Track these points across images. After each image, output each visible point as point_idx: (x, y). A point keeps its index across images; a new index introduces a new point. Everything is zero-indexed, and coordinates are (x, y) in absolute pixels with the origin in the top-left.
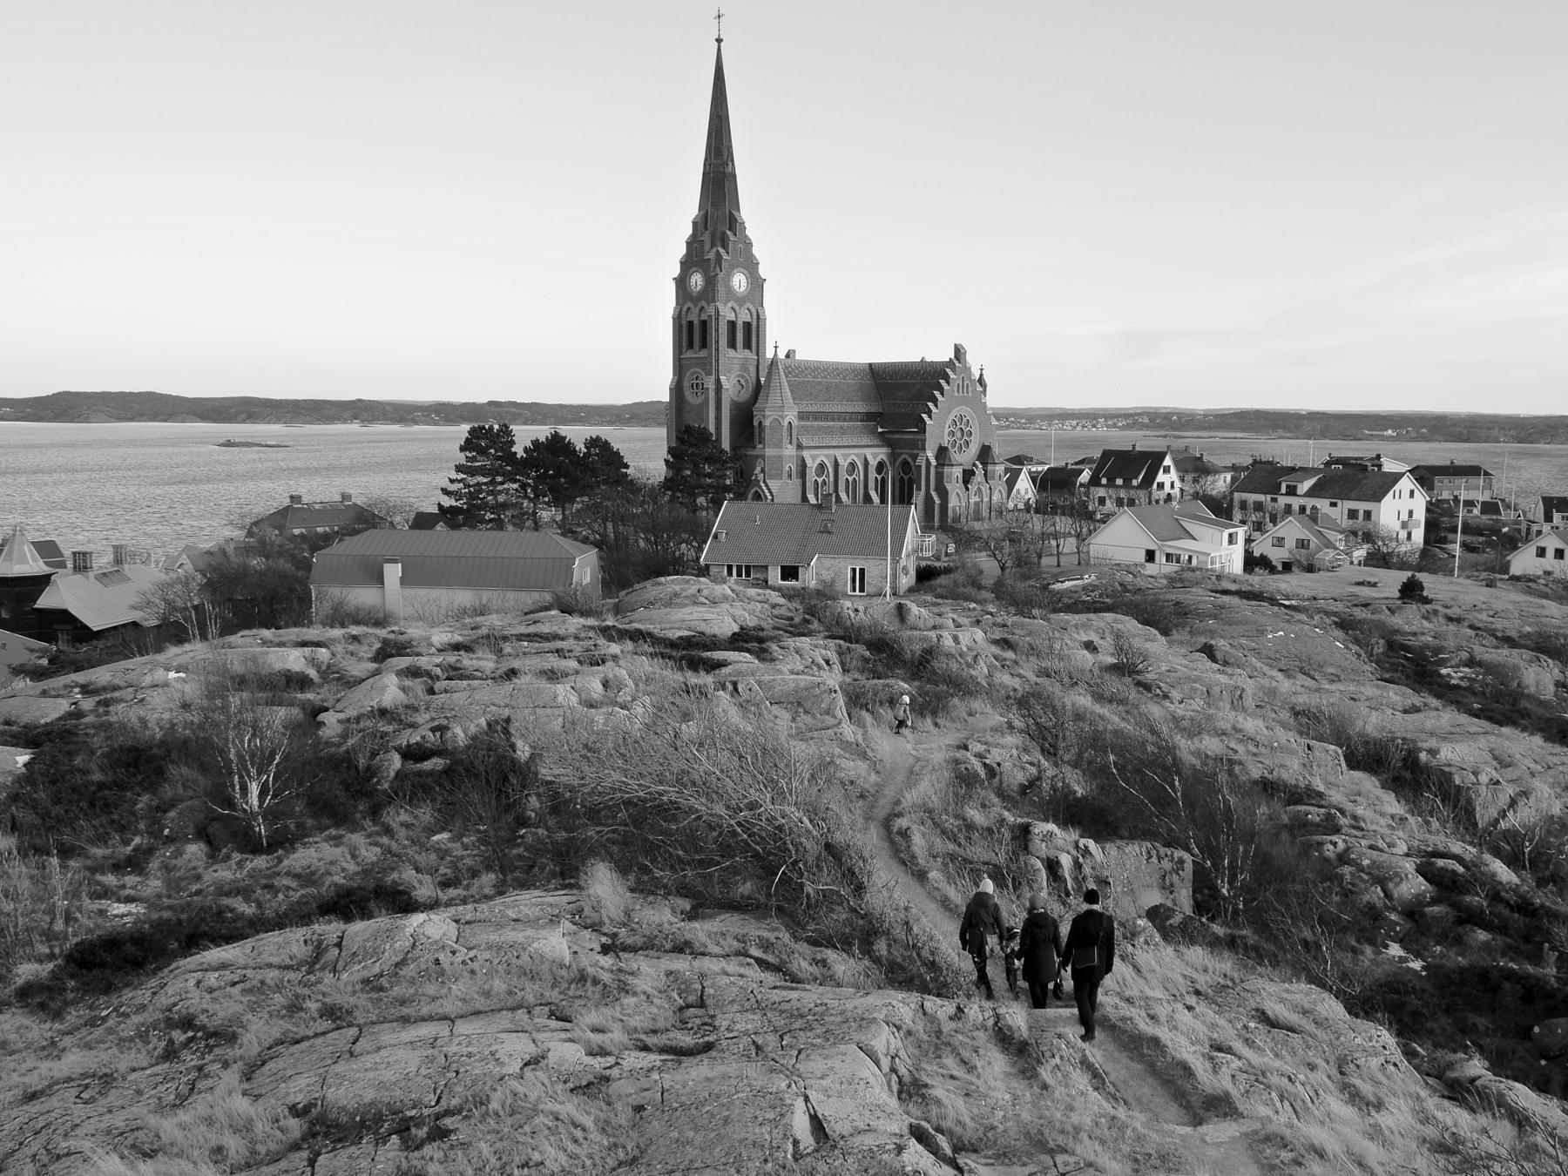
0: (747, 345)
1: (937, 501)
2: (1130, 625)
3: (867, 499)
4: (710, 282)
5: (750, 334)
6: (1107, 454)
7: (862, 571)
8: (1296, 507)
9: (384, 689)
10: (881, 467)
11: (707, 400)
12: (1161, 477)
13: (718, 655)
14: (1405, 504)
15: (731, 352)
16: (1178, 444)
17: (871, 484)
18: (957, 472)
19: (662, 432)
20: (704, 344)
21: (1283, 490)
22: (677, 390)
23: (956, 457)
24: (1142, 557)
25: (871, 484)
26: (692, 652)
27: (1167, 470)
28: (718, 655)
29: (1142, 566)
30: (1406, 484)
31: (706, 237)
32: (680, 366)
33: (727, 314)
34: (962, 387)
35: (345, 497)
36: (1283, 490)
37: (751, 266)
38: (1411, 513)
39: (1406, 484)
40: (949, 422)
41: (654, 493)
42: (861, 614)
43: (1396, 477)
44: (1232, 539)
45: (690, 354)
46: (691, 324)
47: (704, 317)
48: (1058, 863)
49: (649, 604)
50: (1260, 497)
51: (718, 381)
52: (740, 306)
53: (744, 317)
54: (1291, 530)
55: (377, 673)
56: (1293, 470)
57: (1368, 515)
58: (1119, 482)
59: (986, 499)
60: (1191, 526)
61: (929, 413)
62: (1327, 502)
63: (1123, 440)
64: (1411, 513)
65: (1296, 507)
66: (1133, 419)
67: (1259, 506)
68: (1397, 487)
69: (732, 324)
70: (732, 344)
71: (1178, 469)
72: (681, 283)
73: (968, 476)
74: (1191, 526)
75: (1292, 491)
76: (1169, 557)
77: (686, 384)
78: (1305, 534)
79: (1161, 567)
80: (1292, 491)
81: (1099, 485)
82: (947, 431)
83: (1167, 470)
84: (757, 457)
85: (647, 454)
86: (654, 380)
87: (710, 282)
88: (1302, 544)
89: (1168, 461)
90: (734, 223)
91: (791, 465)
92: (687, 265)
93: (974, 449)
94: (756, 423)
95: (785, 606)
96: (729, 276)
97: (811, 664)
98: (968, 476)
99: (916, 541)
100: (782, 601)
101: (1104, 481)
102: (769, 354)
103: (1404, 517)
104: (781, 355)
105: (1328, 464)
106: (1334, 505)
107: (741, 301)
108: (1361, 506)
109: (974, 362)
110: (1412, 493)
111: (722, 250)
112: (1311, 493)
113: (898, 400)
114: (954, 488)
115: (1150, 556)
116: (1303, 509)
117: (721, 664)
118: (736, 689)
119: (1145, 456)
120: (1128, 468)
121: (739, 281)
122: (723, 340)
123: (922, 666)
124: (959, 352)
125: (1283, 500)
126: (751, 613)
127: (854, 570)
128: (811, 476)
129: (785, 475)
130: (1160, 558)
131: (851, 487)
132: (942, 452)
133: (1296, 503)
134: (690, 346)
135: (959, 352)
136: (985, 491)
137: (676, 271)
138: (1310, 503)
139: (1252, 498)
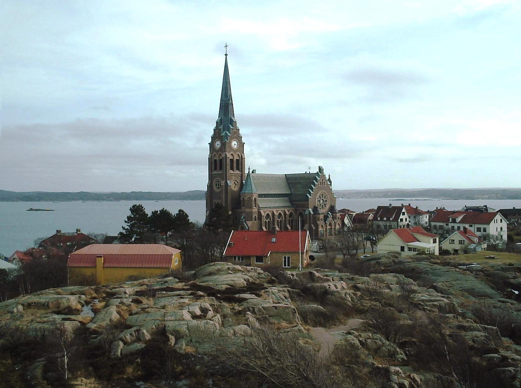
0: (238, 169)
1: (314, 228)
2: (402, 277)
3: (286, 229)
4: (223, 145)
5: (239, 164)
6: (379, 208)
7: (289, 258)
8: (456, 228)
9: (111, 313)
10: (291, 215)
11: (222, 190)
12: (401, 217)
13: (243, 296)
14: (499, 225)
15: (231, 172)
16: (406, 203)
17: (287, 222)
18: (322, 217)
19: (204, 202)
20: (221, 169)
21: (451, 221)
22: (210, 186)
23: (321, 211)
24: (399, 249)
25: (287, 222)
26: (230, 295)
27: (404, 214)
28: (243, 296)
29: (400, 254)
30: (498, 217)
31: (221, 127)
32: (211, 177)
33: (229, 155)
34: (322, 183)
35: (514, 208)
36: (451, 221)
37: (239, 138)
38: (501, 229)
39: (498, 217)
40: (318, 197)
41: (200, 229)
42: (295, 277)
43: (495, 214)
44: (435, 242)
45: (215, 172)
46: (215, 161)
47: (221, 158)
48: (404, 384)
49: (210, 274)
50: (442, 224)
51: (226, 182)
52: (235, 153)
53: (236, 158)
54: (457, 236)
55: (106, 306)
56: (454, 212)
57: (485, 230)
58: (385, 219)
59: (333, 227)
60: (418, 236)
61: (310, 194)
62: (468, 225)
63: (385, 202)
64: (501, 229)
65: (456, 228)
66: (385, 194)
67: (441, 227)
68: (495, 218)
69: (232, 161)
70: (232, 168)
71: (407, 213)
72: (212, 145)
73: (326, 217)
74: (418, 236)
75: (454, 221)
76: (410, 249)
77: (214, 184)
78: (462, 238)
79: (406, 253)
80: (454, 221)
81: (377, 220)
82: (317, 200)
83: (404, 214)
84: (242, 212)
85: (198, 214)
86: (199, 179)
87: (223, 145)
88: (461, 242)
89: (404, 210)
90: (232, 122)
91: (255, 215)
92: (214, 138)
93: (328, 207)
94: (241, 199)
95: (265, 275)
96: (230, 143)
97: (275, 296)
98: (326, 217)
99: (309, 245)
100: (262, 272)
101: (379, 219)
102: (247, 172)
103: (499, 230)
104: (251, 172)
105: (467, 210)
106: (471, 226)
107: (235, 151)
108: (482, 226)
109: (326, 173)
110: (501, 221)
111: (227, 132)
112: (462, 222)
113: (301, 189)
114: (321, 223)
115: (402, 249)
116: (459, 228)
117: (245, 299)
118: (254, 310)
119: (395, 208)
120: (388, 213)
121: (234, 144)
122: (228, 167)
123: (323, 296)
124: (402, 204)
125: (450, 225)
126: (251, 277)
127: (285, 258)
128: (264, 220)
129: (254, 219)
130: (406, 249)
131: (280, 224)
132: (315, 209)
133: (456, 226)
134: (215, 169)
135: (402, 204)
136: (333, 224)
137: (210, 141)
138: (462, 226)
139: (438, 224)
